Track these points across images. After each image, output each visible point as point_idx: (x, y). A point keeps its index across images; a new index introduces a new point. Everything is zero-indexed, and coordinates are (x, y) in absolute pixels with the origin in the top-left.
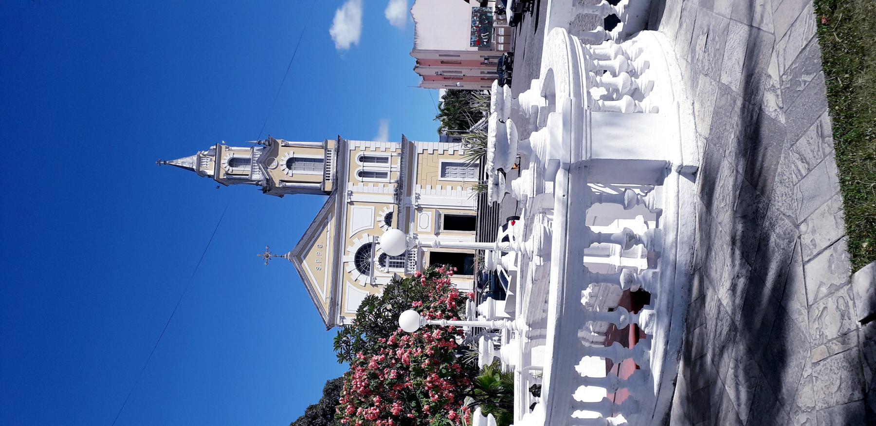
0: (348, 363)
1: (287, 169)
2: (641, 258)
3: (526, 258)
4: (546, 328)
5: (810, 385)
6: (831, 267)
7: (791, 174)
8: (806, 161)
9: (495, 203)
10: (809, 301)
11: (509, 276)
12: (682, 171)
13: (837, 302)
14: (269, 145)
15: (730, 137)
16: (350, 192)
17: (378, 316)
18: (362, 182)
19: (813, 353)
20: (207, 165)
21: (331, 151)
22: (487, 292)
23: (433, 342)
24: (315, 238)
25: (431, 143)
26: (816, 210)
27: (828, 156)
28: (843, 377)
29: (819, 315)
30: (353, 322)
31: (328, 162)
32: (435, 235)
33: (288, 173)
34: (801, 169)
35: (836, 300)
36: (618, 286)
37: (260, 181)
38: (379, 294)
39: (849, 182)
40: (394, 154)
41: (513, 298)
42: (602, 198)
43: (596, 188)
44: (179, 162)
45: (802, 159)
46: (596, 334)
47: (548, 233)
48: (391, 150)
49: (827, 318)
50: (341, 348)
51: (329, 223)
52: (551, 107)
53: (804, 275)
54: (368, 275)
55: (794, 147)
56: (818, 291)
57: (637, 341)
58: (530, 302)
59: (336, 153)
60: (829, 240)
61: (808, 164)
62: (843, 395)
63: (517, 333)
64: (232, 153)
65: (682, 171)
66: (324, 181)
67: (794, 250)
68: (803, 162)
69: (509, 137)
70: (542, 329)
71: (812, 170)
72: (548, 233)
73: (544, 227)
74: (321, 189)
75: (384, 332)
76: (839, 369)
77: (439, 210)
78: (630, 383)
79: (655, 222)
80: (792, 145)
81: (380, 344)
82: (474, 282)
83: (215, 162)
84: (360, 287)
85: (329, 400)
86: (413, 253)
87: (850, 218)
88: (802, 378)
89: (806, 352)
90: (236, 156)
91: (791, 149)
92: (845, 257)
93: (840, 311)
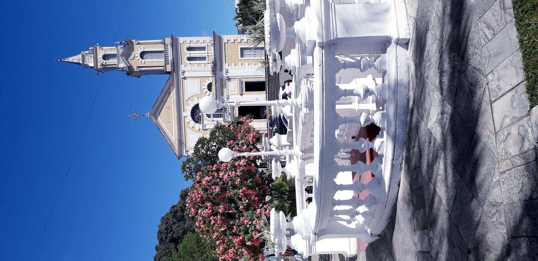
0: (192, 180)
1: (141, 59)
2: (372, 103)
3: (298, 109)
4: (314, 152)
5: (499, 187)
6: (513, 104)
7: (480, 39)
8: (491, 28)
9: (275, 73)
10: (496, 129)
11: (271, 150)
12: (398, 43)
13: (519, 130)
14: (128, 44)
15: (432, 16)
16: (183, 71)
17: (208, 150)
18: (190, 64)
19: (500, 166)
20: (89, 60)
21: (168, 45)
22: (275, 129)
23: (241, 168)
24: (164, 102)
25: (232, 36)
26: (500, 63)
27: (510, 23)
28: (524, 182)
29: (504, 139)
30: (192, 155)
31: (167, 53)
32: (240, 95)
33: (141, 61)
34: (487, 35)
35: (517, 128)
36: (359, 125)
37: (124, 68)
38: (208, 136)
39: (526, 41)
40: (209, 44)
41: (291, 133)
42: (346, 65)
43: (341, 58)
44: (70, 59)
45: (488, 27)
46: (345, 154)
47: (311, 91)
48: (207, 42)
49: (510, 141)
50: (186, 172)
51: (172, 92)
52: (307, 4)
53: (492, 111)
54: (200, 123)
55: (482, 19)
56: (503, 122)
57: (372, 159)
58: (302, 137)
59: (171, 46)
60: (511, 85)
61: (493, 30)
62: (524, 195)
63: (295, 158)
64: (104, 51)
65: (399, 42)
66: (165, 65)
67: (483, 93)
68: (489, 29)
69: (279, 26)
70: (310, 153)
71: (496, 35)
72: (311, 91)
73: (308, 87)
74: (164, 71)
75: (213, 160)
76: (521, 177)
77: (241, 79)
78: (370, 186)
79: (382, 79)
80: (480, 18)
81: (209, 170)
82: (267, 123)
83: (94, 57)
84: (196, 131)
85: (184, 201)
86: (227, 107)
87: (528, 68)
88: (492, 182)
89: (495, 164)
90: (107, 53)
91: (480, 20)
92: (525, 97)
93: (521, 136)
